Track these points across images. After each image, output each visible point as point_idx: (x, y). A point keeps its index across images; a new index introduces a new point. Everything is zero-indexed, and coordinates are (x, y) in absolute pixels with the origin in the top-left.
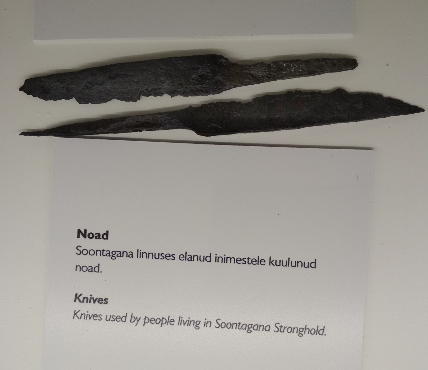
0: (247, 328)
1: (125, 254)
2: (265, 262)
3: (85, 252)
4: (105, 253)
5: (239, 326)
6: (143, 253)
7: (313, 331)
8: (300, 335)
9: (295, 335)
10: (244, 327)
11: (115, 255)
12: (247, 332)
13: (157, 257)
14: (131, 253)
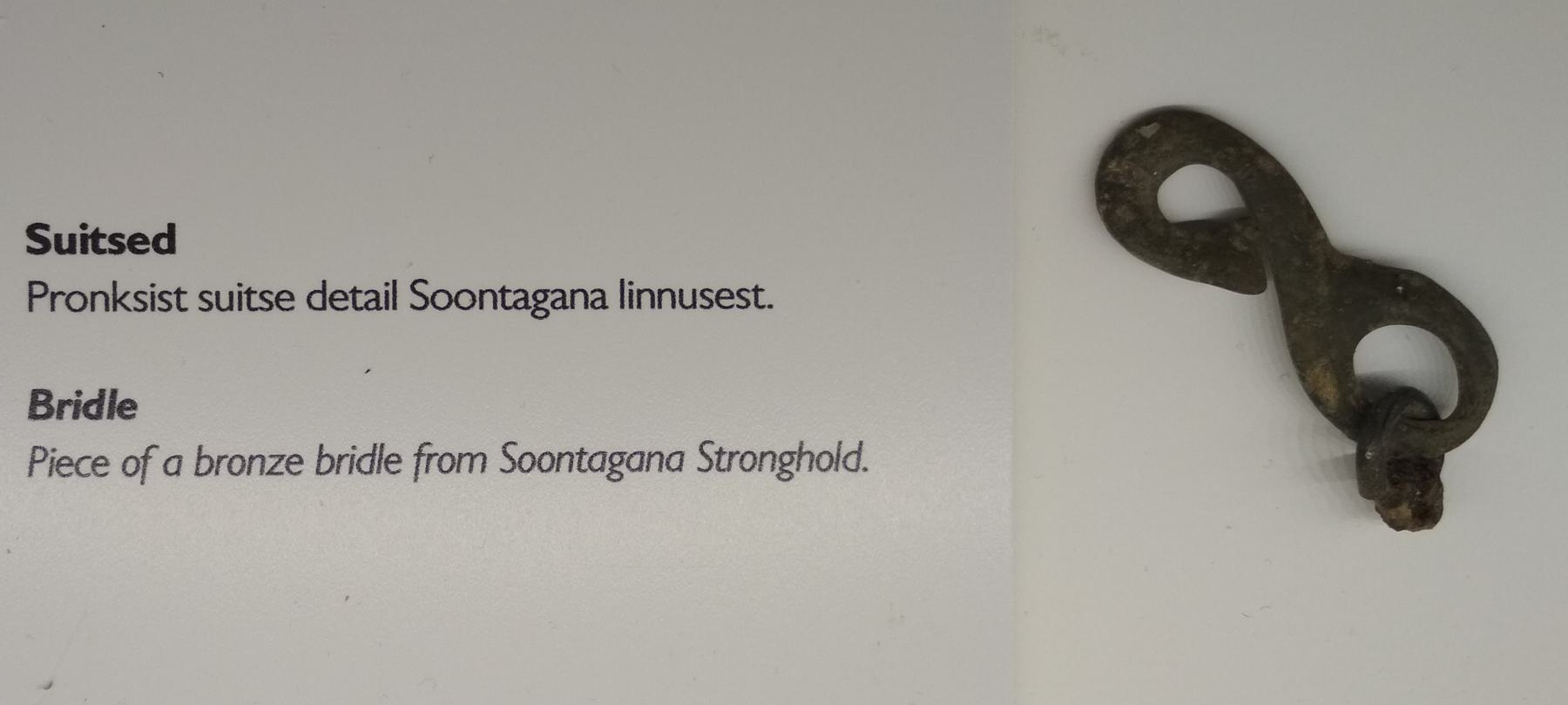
0: (608, 465)
1: (579, 297)
2: (292, 298)
3: (442, 300)
4: (361, 300)
5: (579, 460)
6: (640, 292)
7: (825, 461)
8: (784, 475)
9: (767, 476)
10: (597, 463)
11: (547, 305)
12: (608, 477)
13: (688, 301)
14: (598, 295)
